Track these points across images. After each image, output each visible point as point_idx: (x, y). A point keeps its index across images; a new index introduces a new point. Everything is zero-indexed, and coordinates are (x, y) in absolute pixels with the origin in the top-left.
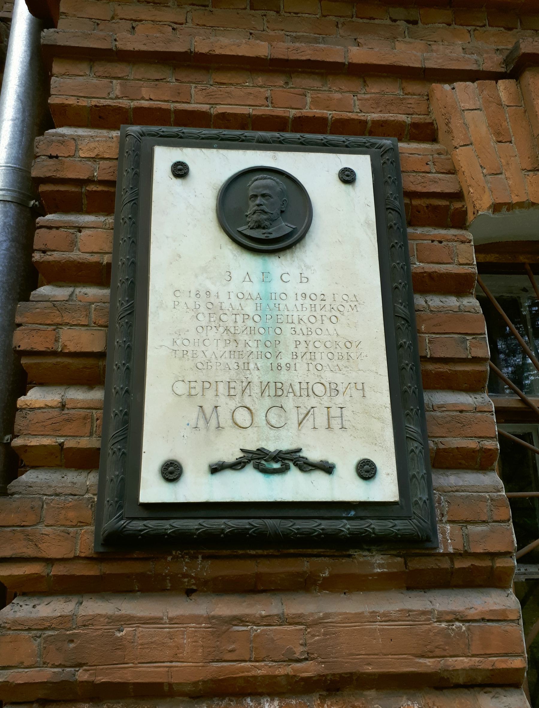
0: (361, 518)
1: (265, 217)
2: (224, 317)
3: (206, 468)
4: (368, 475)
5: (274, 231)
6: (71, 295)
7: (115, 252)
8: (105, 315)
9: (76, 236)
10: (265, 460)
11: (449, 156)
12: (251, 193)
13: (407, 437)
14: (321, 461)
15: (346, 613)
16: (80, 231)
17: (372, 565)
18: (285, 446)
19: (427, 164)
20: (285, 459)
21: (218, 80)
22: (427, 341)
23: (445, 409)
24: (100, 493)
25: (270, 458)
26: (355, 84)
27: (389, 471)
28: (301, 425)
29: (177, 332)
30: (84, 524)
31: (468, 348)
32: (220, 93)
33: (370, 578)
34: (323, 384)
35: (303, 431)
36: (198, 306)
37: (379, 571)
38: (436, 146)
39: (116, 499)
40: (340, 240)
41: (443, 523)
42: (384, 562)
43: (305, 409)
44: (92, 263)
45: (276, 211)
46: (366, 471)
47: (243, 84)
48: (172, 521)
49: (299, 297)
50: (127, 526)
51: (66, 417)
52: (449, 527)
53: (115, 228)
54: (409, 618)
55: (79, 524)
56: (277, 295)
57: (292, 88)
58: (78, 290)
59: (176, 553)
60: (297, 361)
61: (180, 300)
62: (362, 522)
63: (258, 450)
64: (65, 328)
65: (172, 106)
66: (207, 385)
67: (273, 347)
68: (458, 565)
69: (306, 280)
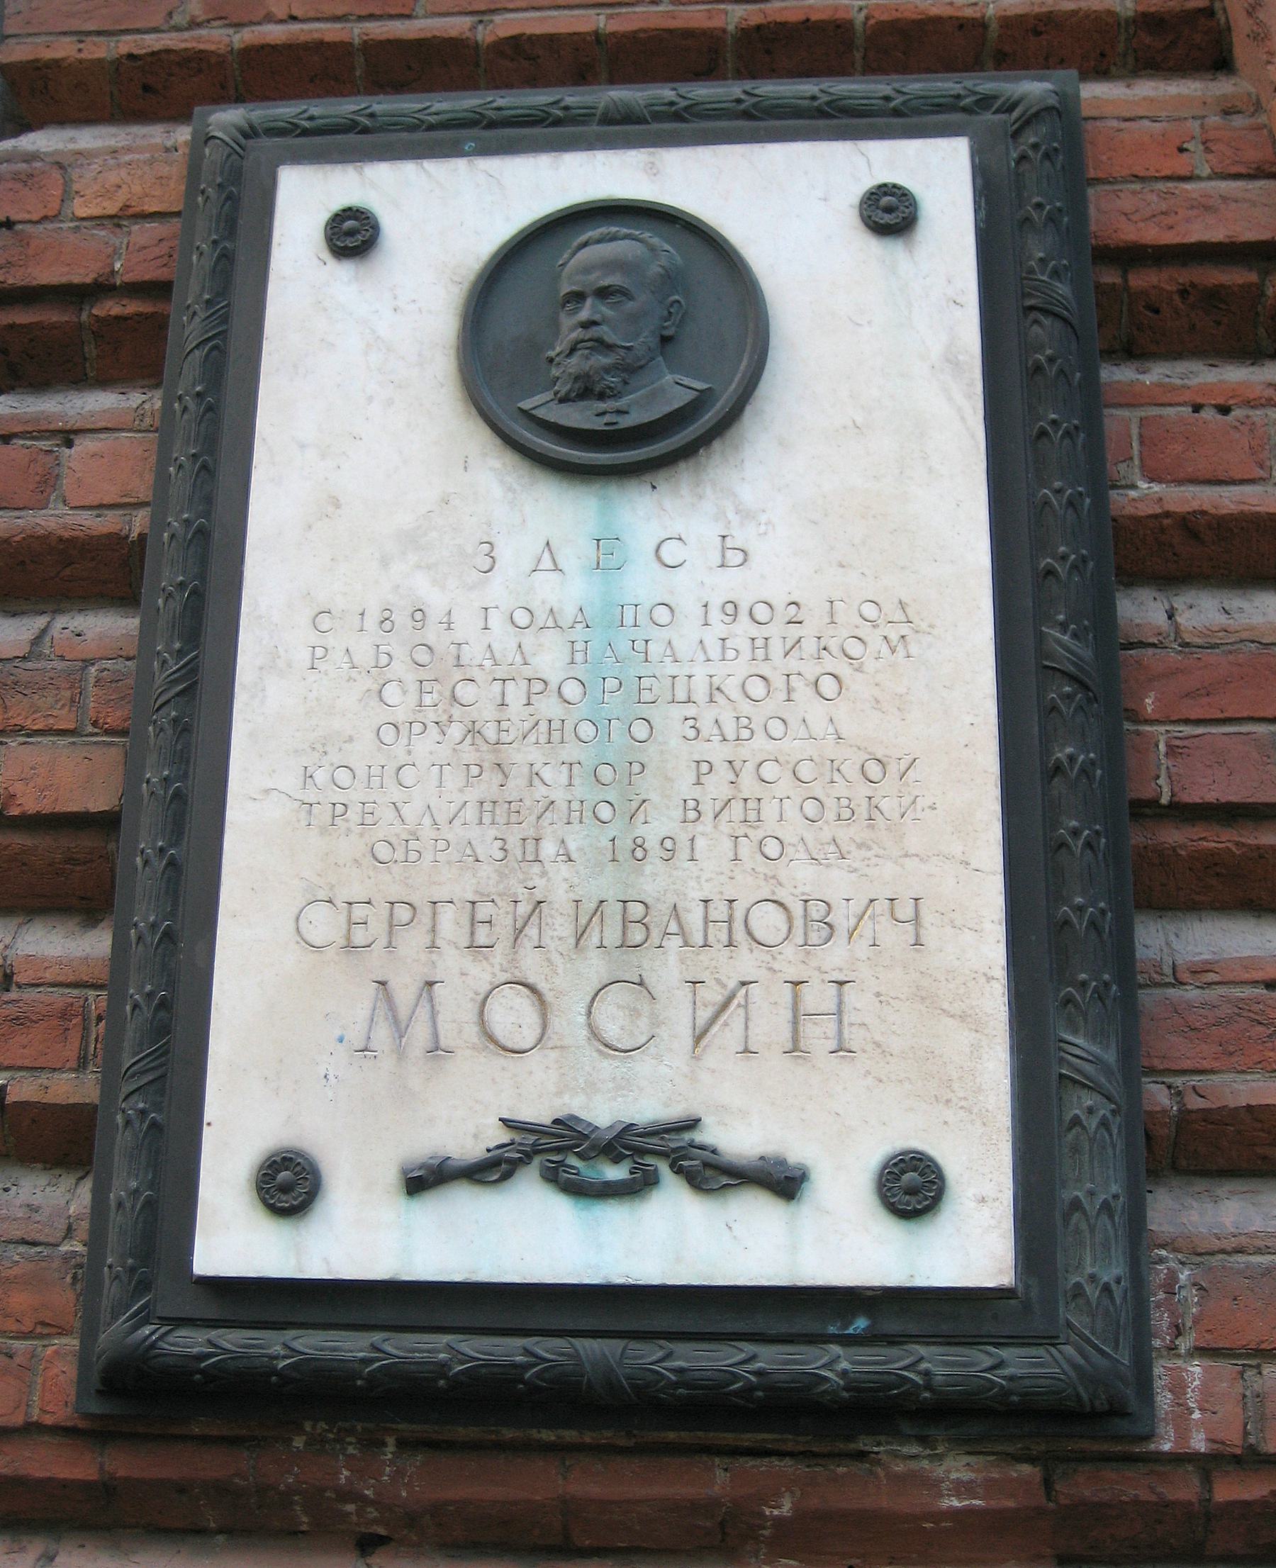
0: (892, 1340)
1: (605, 360)
2: (466, 692)
3: (391, 1176)
4: (914, 1203)
6: (37, 640)
7: (159, 502)
8: (122, 698)
9: (57, 458)
10: (580, 1156)
11: (1263, 119)
12: (565, 288)
13: (1061, 1075)
14: (762, 1158)
16: (69, 444)
17: (933, 1485)
18: (647, 1106)
20: (643, 1152)
22: (1162, 747)
24: (96, 1241)
25: (593, 1147)
27: (988, 1189)
28: (704, 1043)
30: (54, 1330)
34: (781, 904)
35: (711, 1059)
36: (384, 659)
37: (956, 1503)
38: (1223, 87)
39: (130, 1261)
40: (859, 420)
41: (1179, 1356)
42: (973, 1476)
43: (718, 988)
44: (100, 537)
45: (644, 340)
46: (911, 1188)
48: (292, 1333)
49: (715, 615)
50: (161, 1344)
51: (12, 1010)
53: (164, 429)
55: (39, 1330)
58: (61, 621)
59: (314, 1427)
60: (700, 828)
61: (330, 641)
62: (894, 1351)
63: (556, 1121)
65: (356, 31)
66: (403, 913)
67: (620, 783)
68: (1227, 1490)
69: (739, 557)
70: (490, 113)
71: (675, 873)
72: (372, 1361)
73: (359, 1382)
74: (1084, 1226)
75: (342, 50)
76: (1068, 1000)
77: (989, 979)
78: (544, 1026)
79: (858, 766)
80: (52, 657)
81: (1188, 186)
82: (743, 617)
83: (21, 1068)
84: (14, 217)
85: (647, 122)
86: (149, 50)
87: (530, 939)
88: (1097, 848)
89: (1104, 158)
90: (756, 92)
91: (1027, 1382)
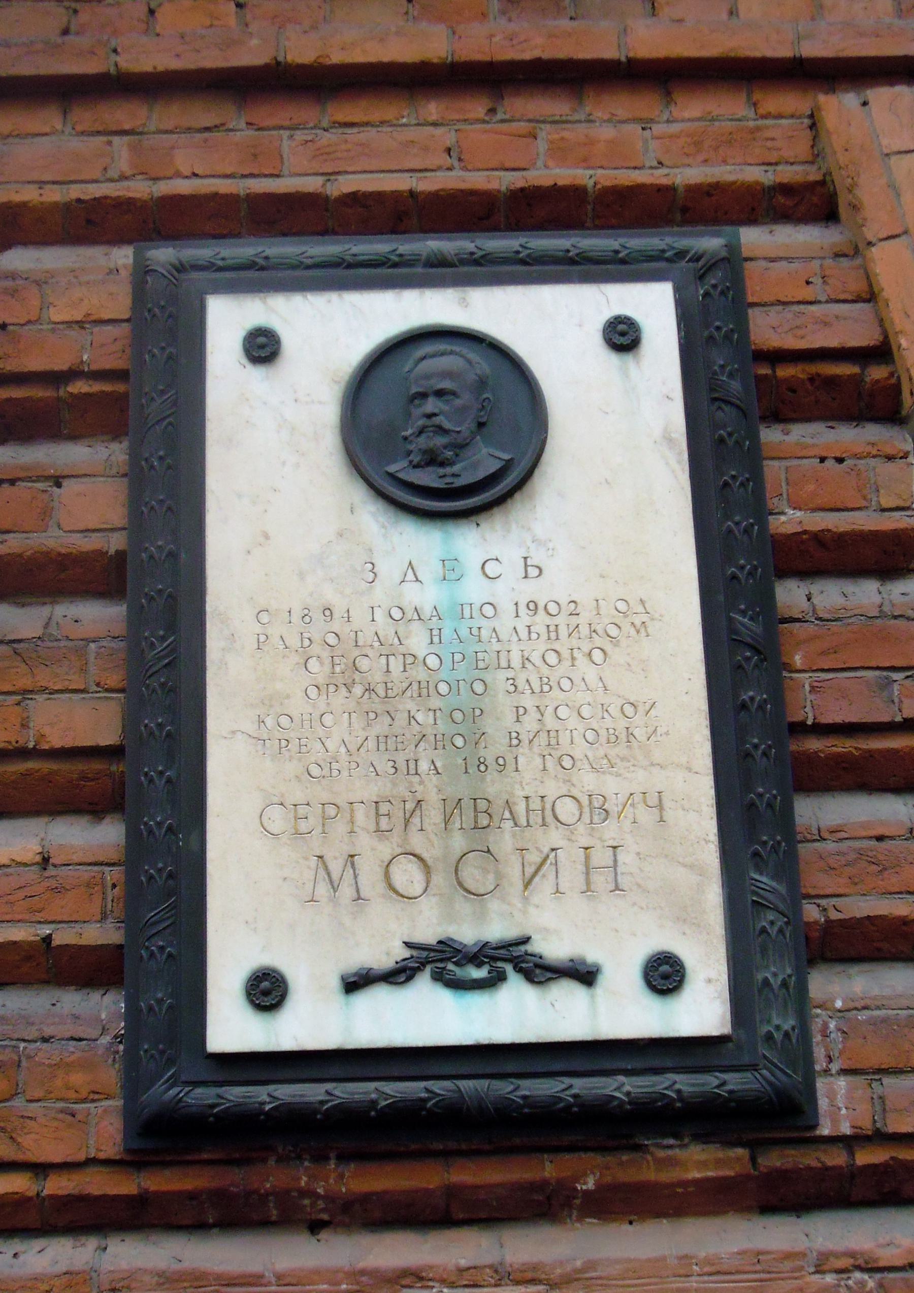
2: (363, 664)
3: (335, 983)
5: (465, 469)
10: (456, 964)
13: (753, 901)
15: (629, 1260)
18: (496, 930)
19: (808, 283)
21: (340, 117)
23: (846, 835)
26: (644, 103)
27: (713, 975)
29: (267, 702)
31: (896, 700)
32: (343, 147)
33: (680, 1190)
41: (832, 1075)
43: (538, 853)
45: (466, 427)
46: (665, 975)
47: (395, 122)
49: (523, 610)
50: (185, 1099)
51: (53, 883)
52: (844, 1083)
54: (758, 1267)
55: (92, 1096)
56: (476, 608)
57: (503, 121)
60: (521, 750)
63: (440, 942)
64: (41, 698)
65: (241, 185)
66: (331, 811)
68: (865, 1157)
69: (537, 572)
70: (348, 258)
71: (506, 780)
72: (327, 1102)
73: (319, 1116)
74: (771, 996)
75: (231, 200)
76: (756, 854)
77: (707, 842)
78: (428, 882)
79: (619, 708)
80: (59, 637)
81: (813, 308)
82: (541, 611)
83: (60, 922)
84: (8, 321)
85: (456, 266)
86: (93, 197)
87: (415, 825)
88: (769, 757)
89: (758, 288)
90: (528, 245)
91: (740, 1094)
